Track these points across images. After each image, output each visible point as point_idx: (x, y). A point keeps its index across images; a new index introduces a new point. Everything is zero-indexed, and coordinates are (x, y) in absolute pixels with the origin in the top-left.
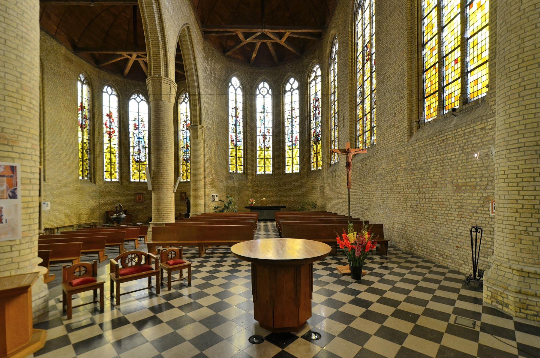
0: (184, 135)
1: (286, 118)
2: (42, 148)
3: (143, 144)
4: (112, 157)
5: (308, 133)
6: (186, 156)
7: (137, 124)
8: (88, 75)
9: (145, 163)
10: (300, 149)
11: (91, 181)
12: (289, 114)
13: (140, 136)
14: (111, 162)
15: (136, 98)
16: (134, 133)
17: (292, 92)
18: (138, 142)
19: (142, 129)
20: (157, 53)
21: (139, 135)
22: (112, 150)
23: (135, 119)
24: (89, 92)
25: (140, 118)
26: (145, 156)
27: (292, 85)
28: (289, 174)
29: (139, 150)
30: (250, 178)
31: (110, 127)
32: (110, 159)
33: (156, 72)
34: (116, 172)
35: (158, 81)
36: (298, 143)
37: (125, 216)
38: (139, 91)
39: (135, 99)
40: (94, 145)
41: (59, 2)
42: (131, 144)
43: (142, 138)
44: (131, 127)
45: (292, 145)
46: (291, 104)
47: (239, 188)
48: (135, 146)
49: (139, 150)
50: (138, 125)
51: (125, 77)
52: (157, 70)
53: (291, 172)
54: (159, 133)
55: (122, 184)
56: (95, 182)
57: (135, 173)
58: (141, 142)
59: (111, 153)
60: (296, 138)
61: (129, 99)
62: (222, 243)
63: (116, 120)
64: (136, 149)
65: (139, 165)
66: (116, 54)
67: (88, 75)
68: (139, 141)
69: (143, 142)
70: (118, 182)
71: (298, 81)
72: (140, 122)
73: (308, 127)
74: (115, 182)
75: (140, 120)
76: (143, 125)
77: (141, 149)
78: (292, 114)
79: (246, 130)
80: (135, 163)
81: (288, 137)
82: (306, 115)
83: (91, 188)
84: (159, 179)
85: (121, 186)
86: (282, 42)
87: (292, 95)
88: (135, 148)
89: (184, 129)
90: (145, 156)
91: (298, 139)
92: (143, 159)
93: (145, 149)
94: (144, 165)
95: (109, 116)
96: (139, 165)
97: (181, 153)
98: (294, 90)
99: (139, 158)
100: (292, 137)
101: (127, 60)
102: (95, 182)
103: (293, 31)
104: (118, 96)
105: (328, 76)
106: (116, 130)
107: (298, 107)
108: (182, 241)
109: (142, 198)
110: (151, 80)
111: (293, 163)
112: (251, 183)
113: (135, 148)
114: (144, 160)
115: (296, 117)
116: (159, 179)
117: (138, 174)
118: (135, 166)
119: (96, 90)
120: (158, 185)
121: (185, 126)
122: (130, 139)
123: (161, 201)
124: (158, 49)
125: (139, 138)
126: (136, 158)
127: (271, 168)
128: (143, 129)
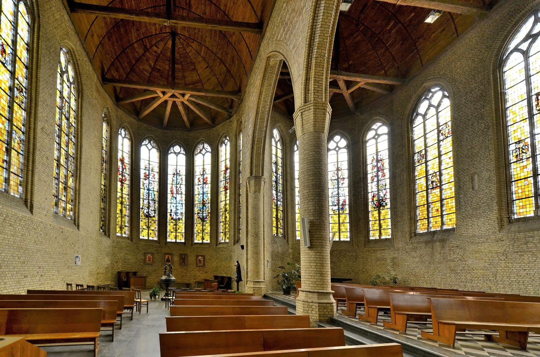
0: (200, 190)
1: (329, 178)
2: (78, 188)
3: (153, 197)
4: (124, 209)
5: (364, 196)
6: (203, 213)
7: (147, 174)
8: (109, 112)
9: (154, 219)
10: (350, 214)
11: (105, 234)
12: (334, 175)
13: (150, 187)
14: (122, 215)
15: (147, 144)
16: (144, 184)
17: (337, 152)
18: (147, 194)
19: (152, 180)
20: (319, 74)
21: (149, 186)
22: (124, 200)
23: (146, 167)
24: (107, 131)
25: (151, 167)
26: (155, 211)
27: (337, 143)
28: (376, 240)
29: (149, 203)
30: (290, 243)
31: (122, 174)
32: (121, 211)
33: (317, 97)
34: (126, 226)
35: (322, 108)
36: (347, 207)
37: (174, 279)
38: (152, 137)
39: (146, 145)
40: (110, 192)
41: (129, 16)
42: (141, 196)
43: (152, 189)
44: (142, 176)
45: (339, 209)
46: (336, 163)
47: (282, 254)
48: (145, 198)
49: (149, 203)
50: (149, 175)
51: (139, 120)
52: (318, 94)
53: (378, 238)
54: (320, 174)
55: (132, 241)
56: (109, 236)
57: (144, 229)
58: (150, 194)
59: (122, 203)
60: (345, 201)
61: (141, 145)
62: (483, 325)
63: (128, 167)
64: (146, 202)
65: (149, 220)
66: (149, 90)
67: (109, 112)
68: (149, 193)
69: (153, 195)
70: (128, 238)
71: (345, 139)
72: (150, 172)
73: (364, 191)
74: (125, 237)
75: (150, 170)
76: (153, 175)
77: (151, 202)
78: (338, 175)
79: (286, 188)
80: (144, 218)
81: (331, 200)
82: (362, 176)
83: (106, 242)
84: (321, 233)
85: (132, 243)
86: (346, 94)
87: (337, 154)
88: (145, 200)
89: (199, 183)
90: (155, 211)
91: (347, 203)
92: (152, 214)
93: (155, 203)
94: (153, 220)
95: (122, 161)
96: (149, 220)
97: (196, 210)
98: (340, 148)
99: (148, 212)
100: (338, 200)
101: (158, 98)
102: (109, 236)
103: (370, 81)
104: (131, 140)
105: (408, 133)
106: (128, 177)
107: (347, 167)
108: (475, 321)
109: (153, 258)
110: (313, 105)
111: (339, 229)
112: (292, 249)
113: (145, 200)
114: (153, 215)
115: (344, 178)
116: (321, 233)
117: (147, 231)
118: (144, 221)
119: (114, 130)
120: (320, 241)
121: (202, 180)
122: (141, 190)
123: (325, 262)
124: (322, 69)
125: (149, 190)
126: (145, 212)
127: (390, 231)
128: (153, 180)
